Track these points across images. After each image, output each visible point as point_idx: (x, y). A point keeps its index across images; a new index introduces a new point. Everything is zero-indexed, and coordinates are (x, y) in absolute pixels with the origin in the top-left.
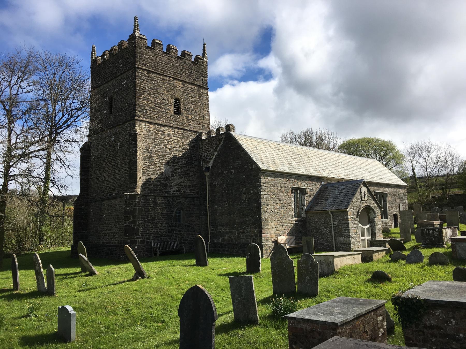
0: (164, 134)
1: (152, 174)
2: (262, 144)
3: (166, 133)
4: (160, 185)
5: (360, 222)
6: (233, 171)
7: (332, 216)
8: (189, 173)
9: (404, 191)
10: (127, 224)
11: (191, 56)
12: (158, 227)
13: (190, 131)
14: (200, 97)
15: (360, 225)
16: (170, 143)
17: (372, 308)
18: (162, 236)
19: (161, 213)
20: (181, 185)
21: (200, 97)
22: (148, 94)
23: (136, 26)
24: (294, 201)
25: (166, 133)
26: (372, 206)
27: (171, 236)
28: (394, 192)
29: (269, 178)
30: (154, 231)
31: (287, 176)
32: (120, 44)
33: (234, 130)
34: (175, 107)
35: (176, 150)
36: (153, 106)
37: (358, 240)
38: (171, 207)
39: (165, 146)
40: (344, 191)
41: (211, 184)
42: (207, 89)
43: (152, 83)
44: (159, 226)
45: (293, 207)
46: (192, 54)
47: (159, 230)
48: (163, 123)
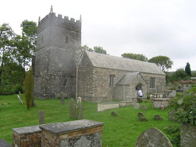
18: (57, 91)
23: (52, 9)
26: (142, 83)
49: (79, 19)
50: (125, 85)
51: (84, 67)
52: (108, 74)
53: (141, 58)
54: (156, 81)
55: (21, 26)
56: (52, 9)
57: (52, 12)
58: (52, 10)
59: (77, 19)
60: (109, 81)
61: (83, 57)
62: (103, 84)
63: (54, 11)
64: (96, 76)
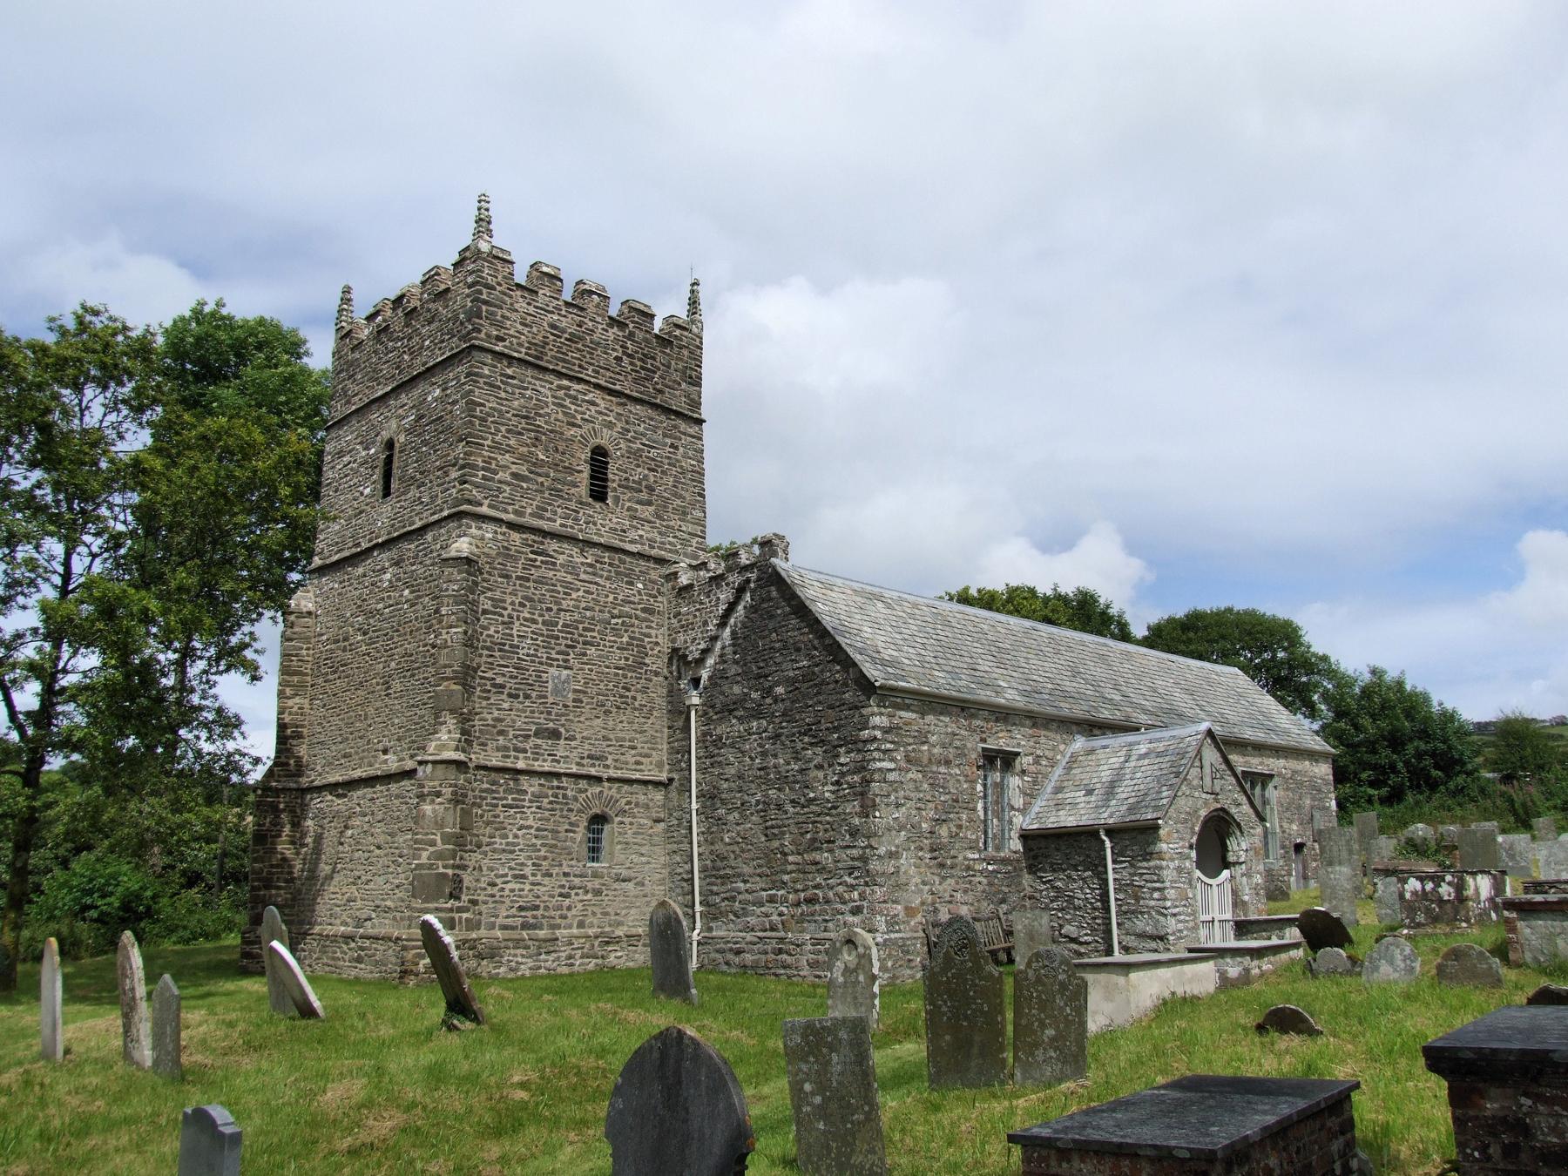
0: (554, 564)
1: (510, 695)
2: (880, 605)
3: (561, 559)
4: (536, 735)
5: (1200, 866)
6: (780, 690)
7: (1108, 844)
8: (634, 698)
9: (1324, 770)
10: (424, 860)
11: (652, 316)
12: (524, 877)
13: (640, 555)
14: (676, 448)
15: (1198, 873)
16: (574, 596)
17: (1318, 1103)
18: (536, 908)
19: (538, 829)
20: (605, 738)
21: (676, 448)
22: (509, 431)
23: (483, 224)
24: (985, 796)
25: (561, 559)
26: (1233, 810)
27: (569, 908)
28: (1295, 772)
29: (902, 713)
30: (512, 890)
31: (963, 709)
32: (431, 277)
33: (785, 551)
34: (592, 477)
35: (593, 618)
36: (523, 470)
37: (1191, 924)
38: (570, 810)
39: (557, 603)
40: (1146, 762)
41: (704, 734)
42: (700, 422)
43: (523, 396)
44: (528, 871)
45: (981, 813)
46: (655, 310)
47: (527, 887)
48: (556, 526)
49: (682, 313)
50: (1110, 832)
51: (768, 692)
52: (974, 746)
53: (1085, 613)
54: (1274, 801)
55: (1374, 672)
56: (483, 224)
57: (484, 247)
58: (490, 232)
59: (667, 308)
60: (980, 806)
61: (751, 609)
62: (944, 831)
63: (502, 238)
64: (892, 760)
